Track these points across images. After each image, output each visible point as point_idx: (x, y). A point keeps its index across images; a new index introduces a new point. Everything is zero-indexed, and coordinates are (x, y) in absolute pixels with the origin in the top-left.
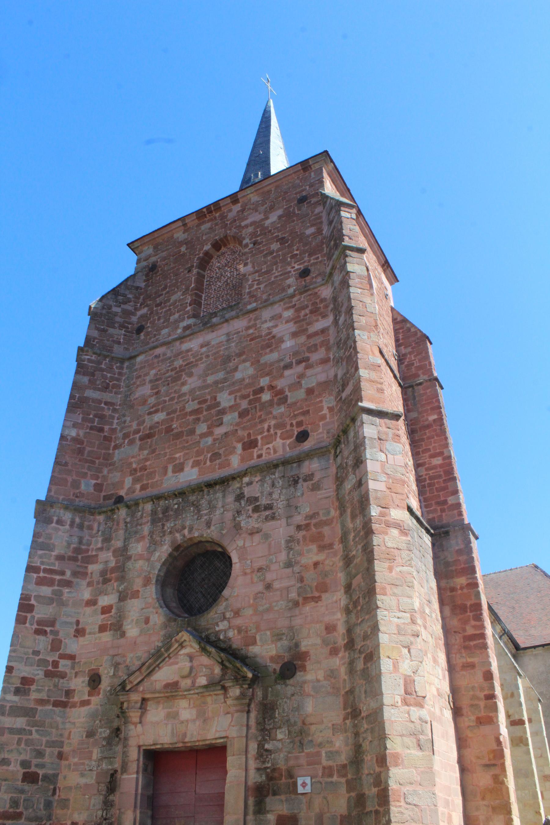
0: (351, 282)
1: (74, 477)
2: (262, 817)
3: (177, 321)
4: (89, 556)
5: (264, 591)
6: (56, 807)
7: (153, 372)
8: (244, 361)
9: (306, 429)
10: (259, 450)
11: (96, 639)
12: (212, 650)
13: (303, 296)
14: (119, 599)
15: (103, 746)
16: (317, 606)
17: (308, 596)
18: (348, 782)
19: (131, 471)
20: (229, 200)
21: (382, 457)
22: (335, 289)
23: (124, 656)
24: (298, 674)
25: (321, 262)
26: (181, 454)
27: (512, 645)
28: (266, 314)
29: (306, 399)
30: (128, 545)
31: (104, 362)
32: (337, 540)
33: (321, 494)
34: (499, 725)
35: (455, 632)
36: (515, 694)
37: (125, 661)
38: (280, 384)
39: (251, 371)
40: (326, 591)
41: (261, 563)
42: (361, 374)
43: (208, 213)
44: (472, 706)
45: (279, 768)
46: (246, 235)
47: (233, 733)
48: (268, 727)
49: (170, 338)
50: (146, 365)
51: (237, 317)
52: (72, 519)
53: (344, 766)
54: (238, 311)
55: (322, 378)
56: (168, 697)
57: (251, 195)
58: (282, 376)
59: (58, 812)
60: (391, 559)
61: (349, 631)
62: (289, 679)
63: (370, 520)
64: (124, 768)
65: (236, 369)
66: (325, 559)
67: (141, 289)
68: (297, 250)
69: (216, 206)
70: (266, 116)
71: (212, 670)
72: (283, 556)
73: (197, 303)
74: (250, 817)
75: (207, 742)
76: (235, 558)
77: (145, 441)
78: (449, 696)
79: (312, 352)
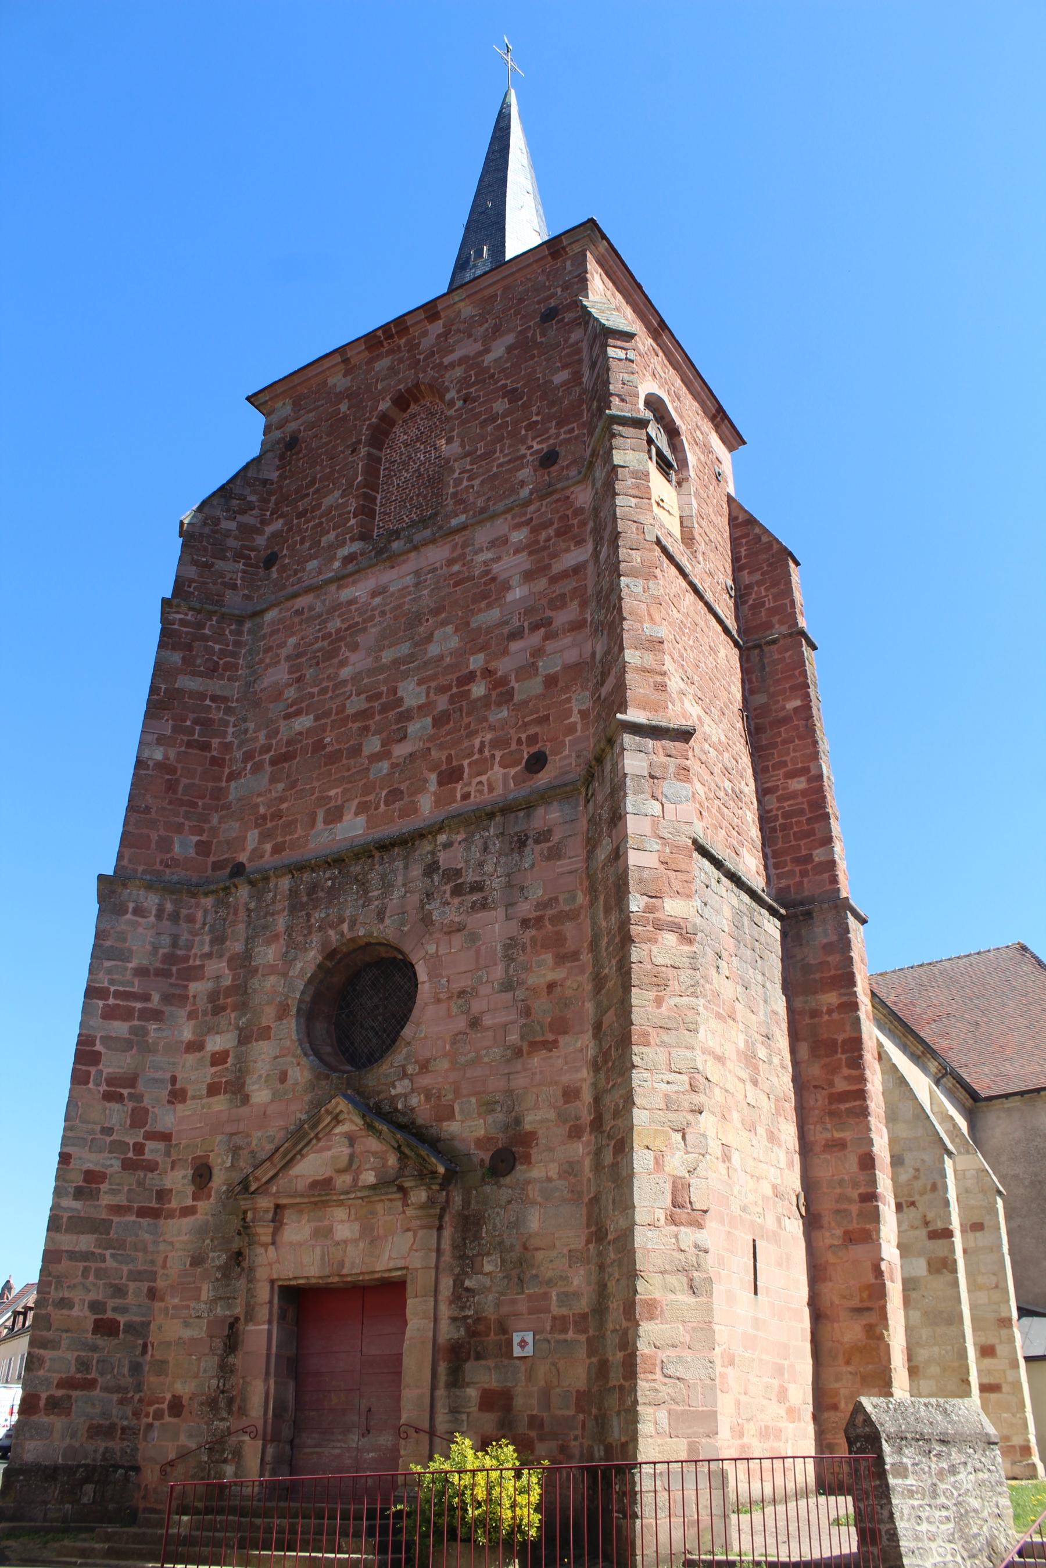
0: (619, 486)
1: (162, 832)
2: (458, 1392)
3: (333, 547)
4: (190, 968)
5: (468, 1031)
6: (149, 1372)
7: (292, 641)
8: (444, 624)
9: (543, 749)
10: (466, 785)
12: (384, 1128)
13: (544, 503)
14: (239, 1041)
15: (217, 1280)
16: (550, 1058)
17: (539, 1039)
19: (257, 819)
21: (655, 808)
22: (596, 493)
23: (248, 1136)
24: (519, 1167)
25: (577, 437)
26: (339, 790)
27: (964, 1092)
28: (483, 535)
29: (544, 695)
31: (209, 623)
32: (585, 945)
33: (563, 865)
35: (815, 1087)
37: (249, 1144)
38: (503, 666)
39: (454, 642)
40: (566, 1033)
42: (627, 659)
43: (386, 339)
44: (838, 1211)
45: (486, 1317)
46: (452, 382)
47: (416, 1261)
48: (470, 1253)
49: (321, 577)
50: (281, 627)
51: (433, 541)
52: (159, 905)
53: (584, 1316)
55: (571, 656)
56: (316, 1203)
57: (463, 304)
58: (505, 652)
59: (151, 1379)
61: (597, 1100)
62: (504, 1176)
63: (629, 918)
64: (250, 1315)
65: (429, 639)
66: (565, 979)
67: (272, 484)
68: (537, 414)
69: (399, 326)
70: (502, 125)
71: (385, 1160)
72: (498, 972)
73: (367, 511)
74: (441, 1392)
75: (377, 1276)
76: (422, 975)
77: (280, 766)
78: (798, 1196)
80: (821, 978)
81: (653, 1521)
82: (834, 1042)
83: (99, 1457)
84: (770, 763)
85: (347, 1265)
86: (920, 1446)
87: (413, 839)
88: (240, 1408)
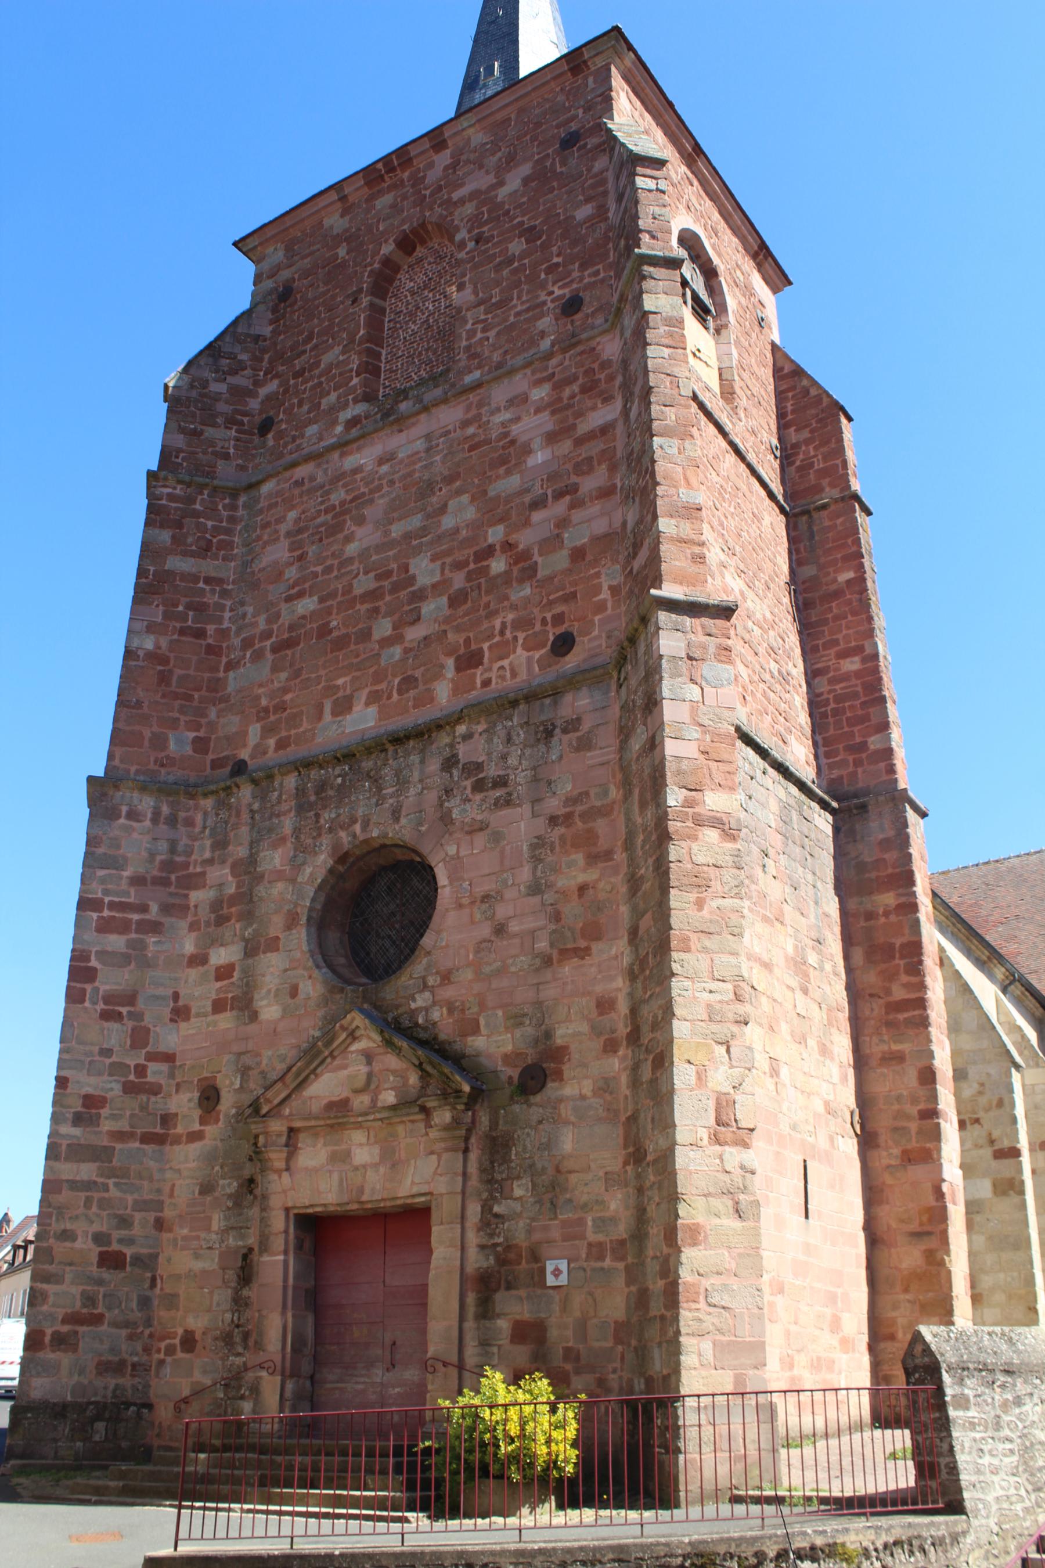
0: (650, 335)
1: (156, 729)
2: (487, 1323)
3: (334, 410)
7: (292, 515)
8: (459, 492)
10: (486, 671)
11: (208, 1026)
12: (404, 1044)
13: (567, 355)
15: (229, 1208)
17: (569, 946)
18: (627, 1268)
19: (258, 712)
20: (426, 144)
22: (625, 344)
23: (258, 1055)
24: (550, 1085)
25: (602, 281)
26: (348, 679)
28: (500, 394)
30: (257, 853)
32: (619, 843)
33: (593, 757)
34: (941, 1165)
35: (871, 995)
36: (1006, 1101)
37: (259, 1064)
38: (525, 539)
39: (471, 513)
40: (598, 938)
41: (487, 886)
42: (661, 528)
43: (387, 172)
44: (896, 1129)
45: (516, 1246)
47: (441, 1186)
48: (498, 1177)
49: (323, 444)
51: (445, 401)
53: (622, 1243)
54: (447, 387)
55: (600, 527)
56: (332, 1126)
57: (471, 131)
58: (527, 523)
59: (162, 1313)
60: (701, 884)
61: (634, 1011)
62: (534, 1093)
63: (666, 813)
64: (264, 1246)
65: (443, 509)
66: (599, 880)
67: (265, 340)
68: (558, 255)
71: (405, 1079)
72: (525, 874)
74: (470, 1324)
75: (399, 1202)
76: (442, 878)
77: (283, 653)
78: (852, 1113)
79: (584, 473)
80: (878, 877)
81: (697, 1456)
82: (892, 946)
83: (109, 1394)
84: (820, 642)
85: (367, 1191)
86: (983, 1377)
87: (430, 731)
88: (256, 1342)
